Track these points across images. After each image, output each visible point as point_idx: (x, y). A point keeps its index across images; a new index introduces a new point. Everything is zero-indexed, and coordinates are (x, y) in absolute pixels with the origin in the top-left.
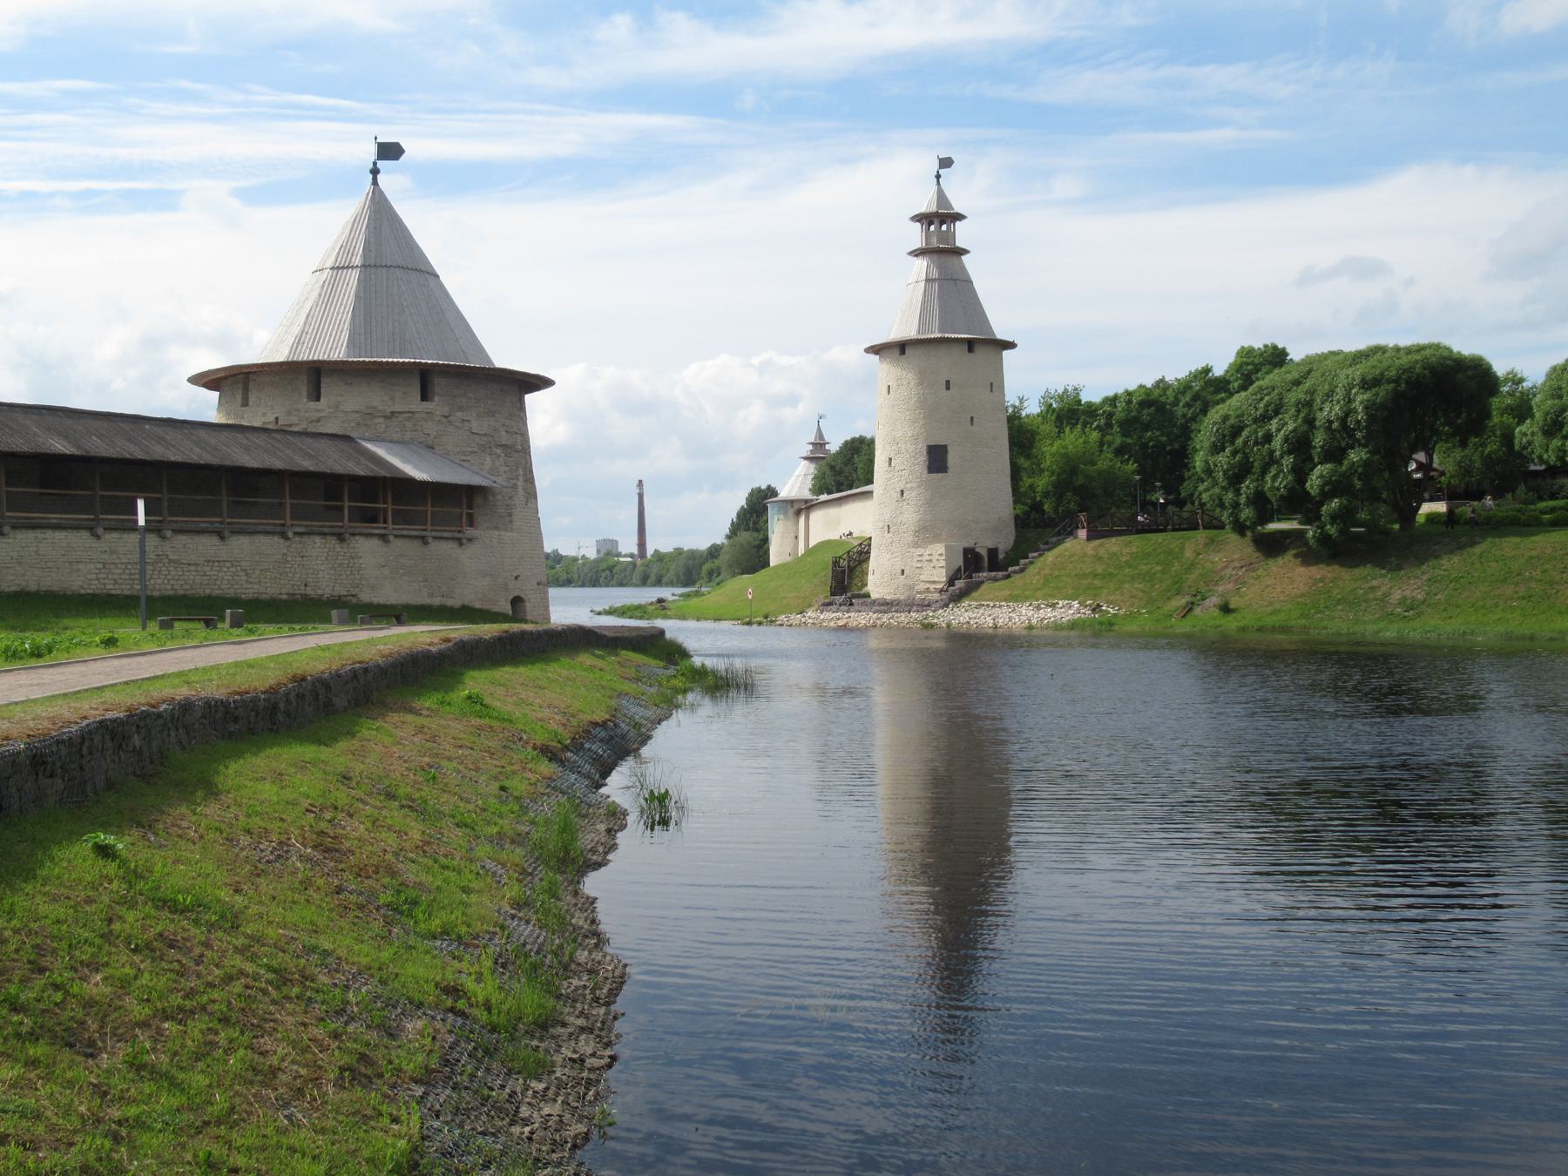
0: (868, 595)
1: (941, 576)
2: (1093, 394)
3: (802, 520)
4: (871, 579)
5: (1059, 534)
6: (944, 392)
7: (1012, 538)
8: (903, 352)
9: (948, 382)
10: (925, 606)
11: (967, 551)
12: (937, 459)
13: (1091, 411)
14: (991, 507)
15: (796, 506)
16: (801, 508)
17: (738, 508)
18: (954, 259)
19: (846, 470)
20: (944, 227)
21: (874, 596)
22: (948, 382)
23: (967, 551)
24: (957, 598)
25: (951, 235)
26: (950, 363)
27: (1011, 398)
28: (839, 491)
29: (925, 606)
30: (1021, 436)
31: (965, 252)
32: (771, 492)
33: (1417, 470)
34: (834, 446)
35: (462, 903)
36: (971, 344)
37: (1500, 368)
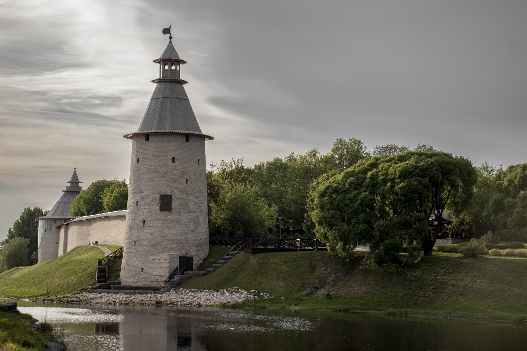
0: (119, 283)
1: (165, 273)
2: (249, 164)
3: (63, 230)
4: (122, 273)
5: (235, 249)
6: (171, 164)
7: (207, 251)
8: (147, 139)
9: (173, 158)
10: (156, 290)
11: (182, 259)
12: (166, 202)
13: (249, 172)
14: (191, 229)
15: (59, 223)
16: (60, 223)
17: (15, 221)
18: (179, 86)
19: (97, 201)
20: (173, 68)
21: (123, 284)
22: (173, 158)
23: (182, 259)
24: (177, 286)
25: (177, 73)
26: (173, 147)
27: (208, 168)
28: (89, 214)
29: (156, 290)
30: (213, 191)
31: (186, 82)
32: (38, 212)
33: (439, 217)
34: (85, 185)
35: (382, 240)
36: (187, 137)
37: (477, 164)
